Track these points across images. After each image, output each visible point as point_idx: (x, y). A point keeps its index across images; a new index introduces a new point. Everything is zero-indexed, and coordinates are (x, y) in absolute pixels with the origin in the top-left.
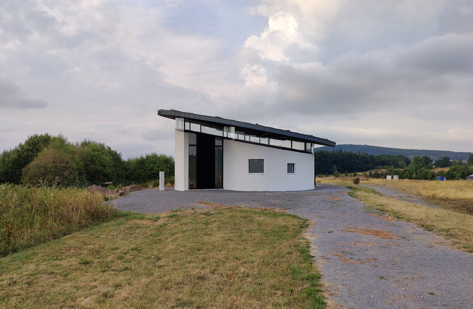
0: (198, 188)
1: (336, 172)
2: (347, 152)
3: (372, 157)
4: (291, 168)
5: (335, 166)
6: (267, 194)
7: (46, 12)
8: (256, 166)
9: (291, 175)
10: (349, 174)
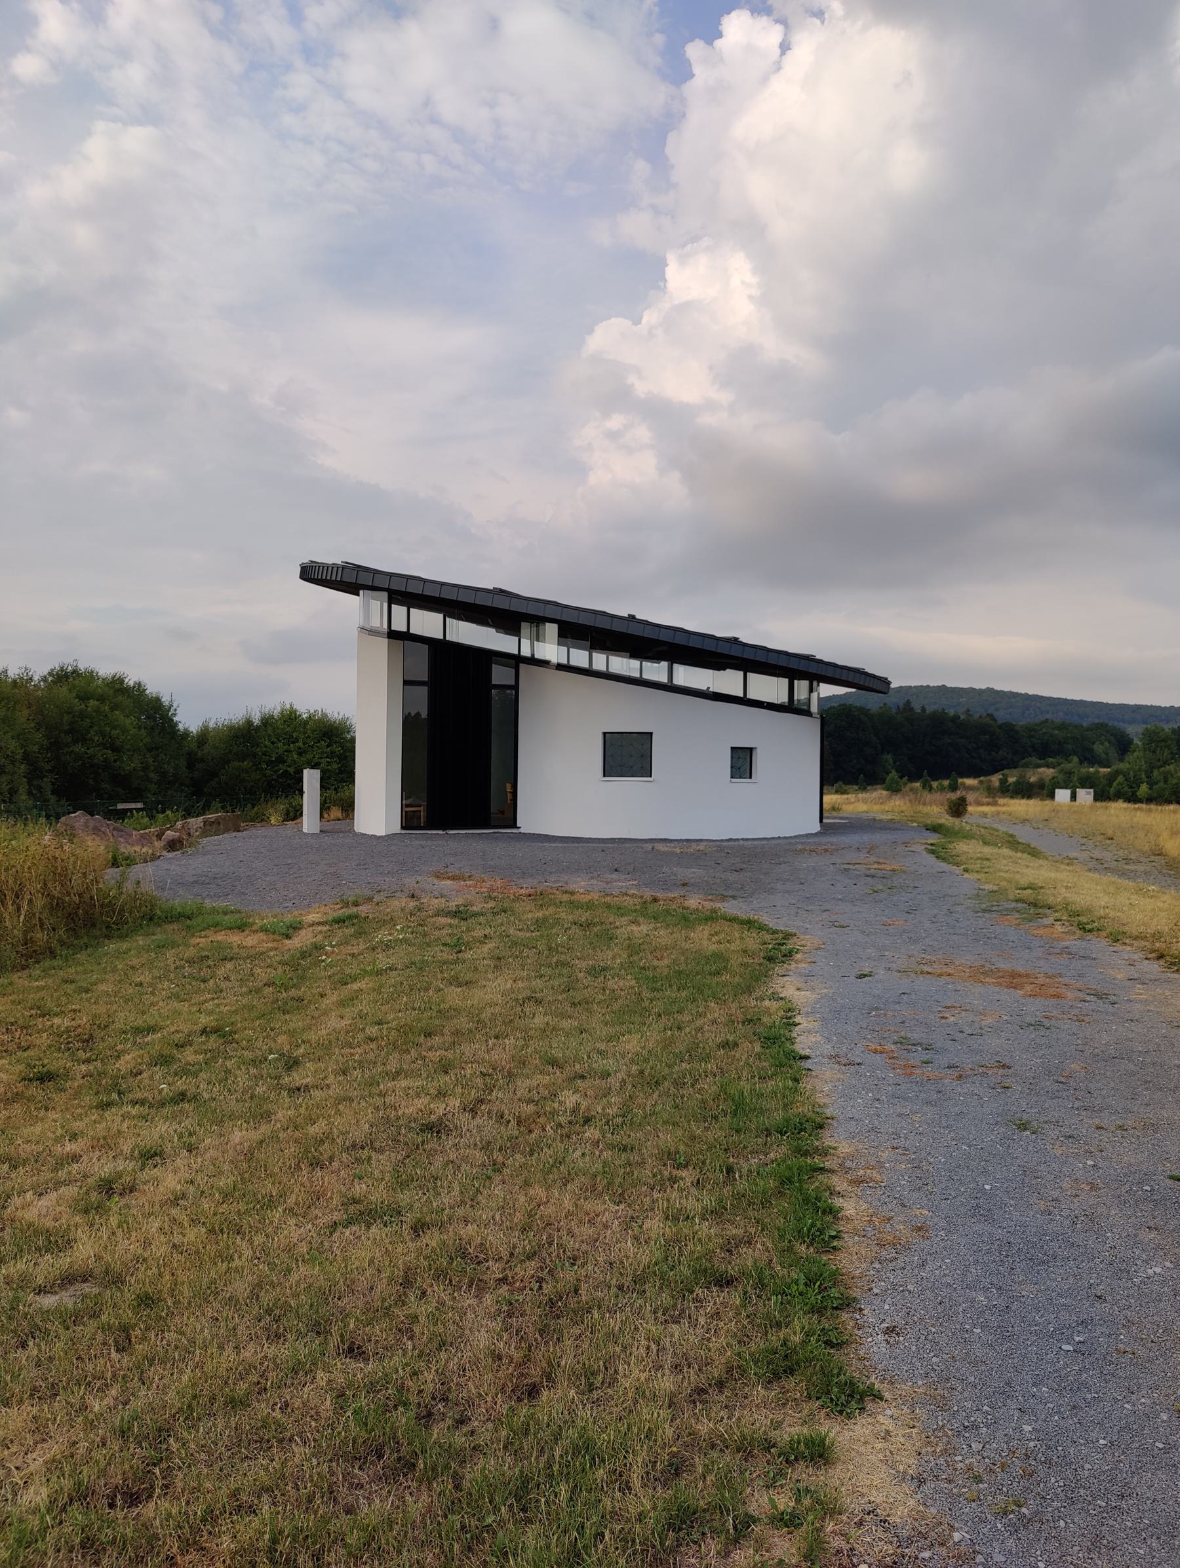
0: (430, 825)
1: (894, 774)
3: (1008, 728)
4: (742, 762)
5: (889, 757)
8: (627, 755)
10: (935, 784)
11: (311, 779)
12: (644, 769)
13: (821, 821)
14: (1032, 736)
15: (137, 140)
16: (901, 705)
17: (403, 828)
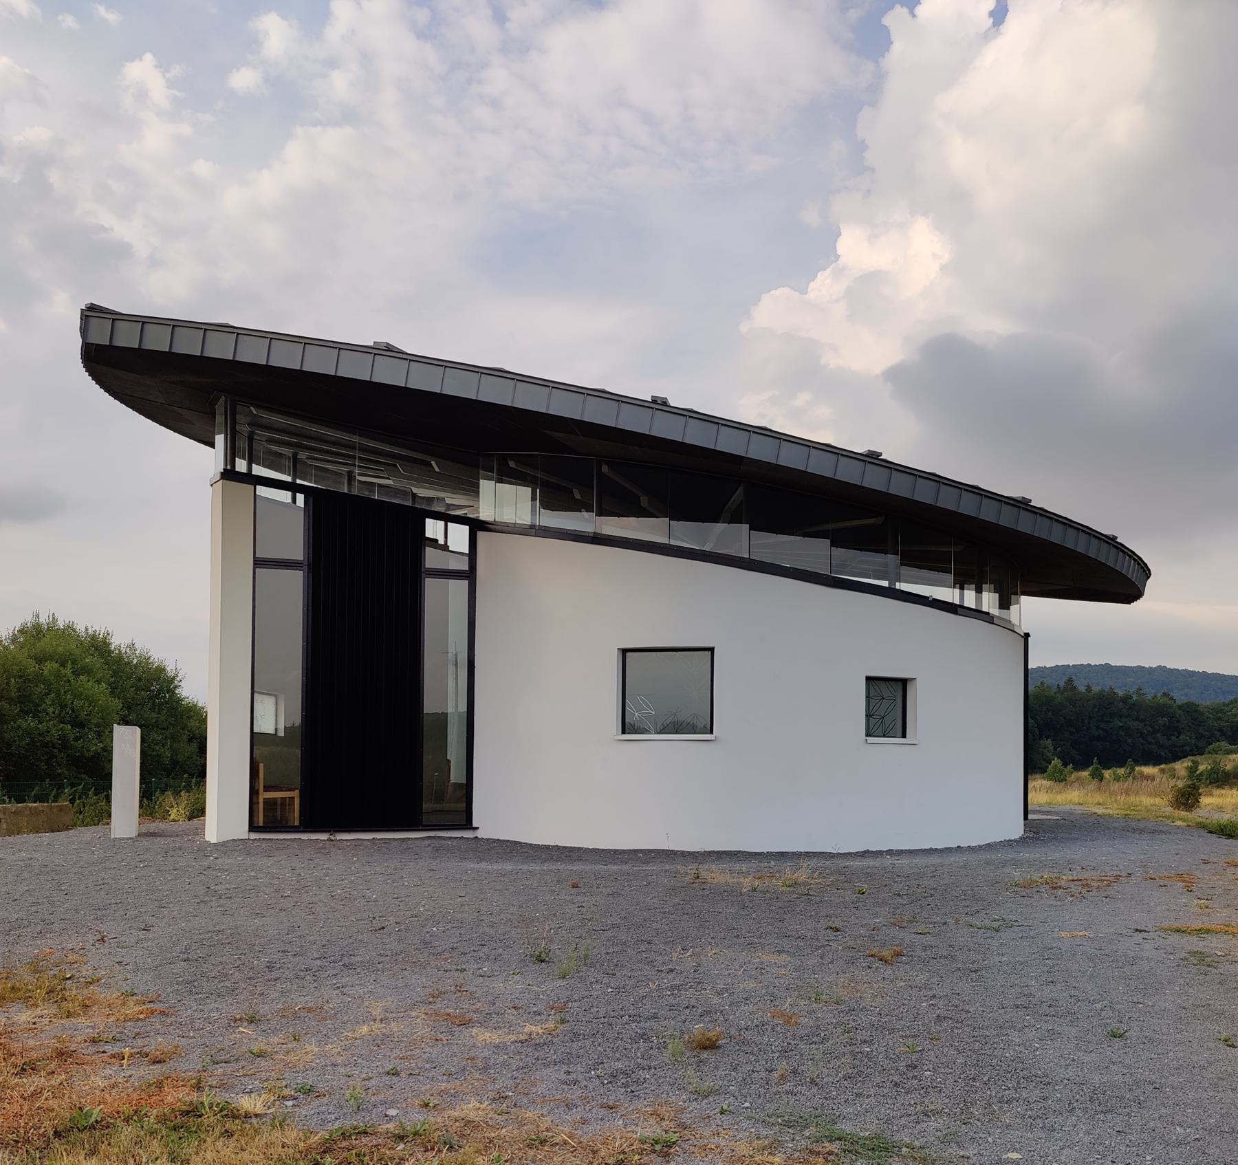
0: (309, 825)
1: (1056, 762)
2: (1096, 689)
3: (1191, 710)
4: (888, 704)
5: (1049, 742)
6: (716, 875)
7: (103, 229)
9: (888, 747)
10: (1107, 774)
11: (126, 746)
12: (694, 721)
13: (1026, 818)
14: (1220, 719)
15: (333, 140)
16: (1062, 684)
17: (253, 828)
